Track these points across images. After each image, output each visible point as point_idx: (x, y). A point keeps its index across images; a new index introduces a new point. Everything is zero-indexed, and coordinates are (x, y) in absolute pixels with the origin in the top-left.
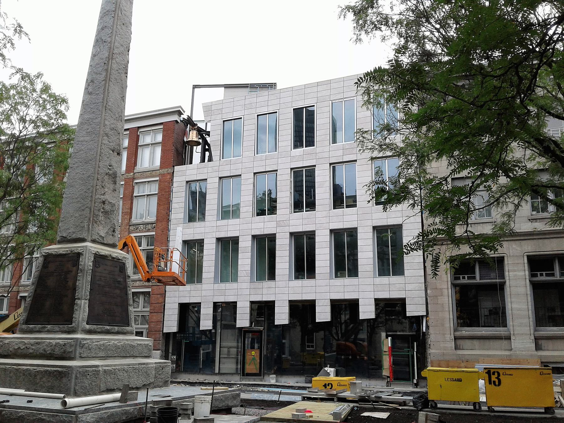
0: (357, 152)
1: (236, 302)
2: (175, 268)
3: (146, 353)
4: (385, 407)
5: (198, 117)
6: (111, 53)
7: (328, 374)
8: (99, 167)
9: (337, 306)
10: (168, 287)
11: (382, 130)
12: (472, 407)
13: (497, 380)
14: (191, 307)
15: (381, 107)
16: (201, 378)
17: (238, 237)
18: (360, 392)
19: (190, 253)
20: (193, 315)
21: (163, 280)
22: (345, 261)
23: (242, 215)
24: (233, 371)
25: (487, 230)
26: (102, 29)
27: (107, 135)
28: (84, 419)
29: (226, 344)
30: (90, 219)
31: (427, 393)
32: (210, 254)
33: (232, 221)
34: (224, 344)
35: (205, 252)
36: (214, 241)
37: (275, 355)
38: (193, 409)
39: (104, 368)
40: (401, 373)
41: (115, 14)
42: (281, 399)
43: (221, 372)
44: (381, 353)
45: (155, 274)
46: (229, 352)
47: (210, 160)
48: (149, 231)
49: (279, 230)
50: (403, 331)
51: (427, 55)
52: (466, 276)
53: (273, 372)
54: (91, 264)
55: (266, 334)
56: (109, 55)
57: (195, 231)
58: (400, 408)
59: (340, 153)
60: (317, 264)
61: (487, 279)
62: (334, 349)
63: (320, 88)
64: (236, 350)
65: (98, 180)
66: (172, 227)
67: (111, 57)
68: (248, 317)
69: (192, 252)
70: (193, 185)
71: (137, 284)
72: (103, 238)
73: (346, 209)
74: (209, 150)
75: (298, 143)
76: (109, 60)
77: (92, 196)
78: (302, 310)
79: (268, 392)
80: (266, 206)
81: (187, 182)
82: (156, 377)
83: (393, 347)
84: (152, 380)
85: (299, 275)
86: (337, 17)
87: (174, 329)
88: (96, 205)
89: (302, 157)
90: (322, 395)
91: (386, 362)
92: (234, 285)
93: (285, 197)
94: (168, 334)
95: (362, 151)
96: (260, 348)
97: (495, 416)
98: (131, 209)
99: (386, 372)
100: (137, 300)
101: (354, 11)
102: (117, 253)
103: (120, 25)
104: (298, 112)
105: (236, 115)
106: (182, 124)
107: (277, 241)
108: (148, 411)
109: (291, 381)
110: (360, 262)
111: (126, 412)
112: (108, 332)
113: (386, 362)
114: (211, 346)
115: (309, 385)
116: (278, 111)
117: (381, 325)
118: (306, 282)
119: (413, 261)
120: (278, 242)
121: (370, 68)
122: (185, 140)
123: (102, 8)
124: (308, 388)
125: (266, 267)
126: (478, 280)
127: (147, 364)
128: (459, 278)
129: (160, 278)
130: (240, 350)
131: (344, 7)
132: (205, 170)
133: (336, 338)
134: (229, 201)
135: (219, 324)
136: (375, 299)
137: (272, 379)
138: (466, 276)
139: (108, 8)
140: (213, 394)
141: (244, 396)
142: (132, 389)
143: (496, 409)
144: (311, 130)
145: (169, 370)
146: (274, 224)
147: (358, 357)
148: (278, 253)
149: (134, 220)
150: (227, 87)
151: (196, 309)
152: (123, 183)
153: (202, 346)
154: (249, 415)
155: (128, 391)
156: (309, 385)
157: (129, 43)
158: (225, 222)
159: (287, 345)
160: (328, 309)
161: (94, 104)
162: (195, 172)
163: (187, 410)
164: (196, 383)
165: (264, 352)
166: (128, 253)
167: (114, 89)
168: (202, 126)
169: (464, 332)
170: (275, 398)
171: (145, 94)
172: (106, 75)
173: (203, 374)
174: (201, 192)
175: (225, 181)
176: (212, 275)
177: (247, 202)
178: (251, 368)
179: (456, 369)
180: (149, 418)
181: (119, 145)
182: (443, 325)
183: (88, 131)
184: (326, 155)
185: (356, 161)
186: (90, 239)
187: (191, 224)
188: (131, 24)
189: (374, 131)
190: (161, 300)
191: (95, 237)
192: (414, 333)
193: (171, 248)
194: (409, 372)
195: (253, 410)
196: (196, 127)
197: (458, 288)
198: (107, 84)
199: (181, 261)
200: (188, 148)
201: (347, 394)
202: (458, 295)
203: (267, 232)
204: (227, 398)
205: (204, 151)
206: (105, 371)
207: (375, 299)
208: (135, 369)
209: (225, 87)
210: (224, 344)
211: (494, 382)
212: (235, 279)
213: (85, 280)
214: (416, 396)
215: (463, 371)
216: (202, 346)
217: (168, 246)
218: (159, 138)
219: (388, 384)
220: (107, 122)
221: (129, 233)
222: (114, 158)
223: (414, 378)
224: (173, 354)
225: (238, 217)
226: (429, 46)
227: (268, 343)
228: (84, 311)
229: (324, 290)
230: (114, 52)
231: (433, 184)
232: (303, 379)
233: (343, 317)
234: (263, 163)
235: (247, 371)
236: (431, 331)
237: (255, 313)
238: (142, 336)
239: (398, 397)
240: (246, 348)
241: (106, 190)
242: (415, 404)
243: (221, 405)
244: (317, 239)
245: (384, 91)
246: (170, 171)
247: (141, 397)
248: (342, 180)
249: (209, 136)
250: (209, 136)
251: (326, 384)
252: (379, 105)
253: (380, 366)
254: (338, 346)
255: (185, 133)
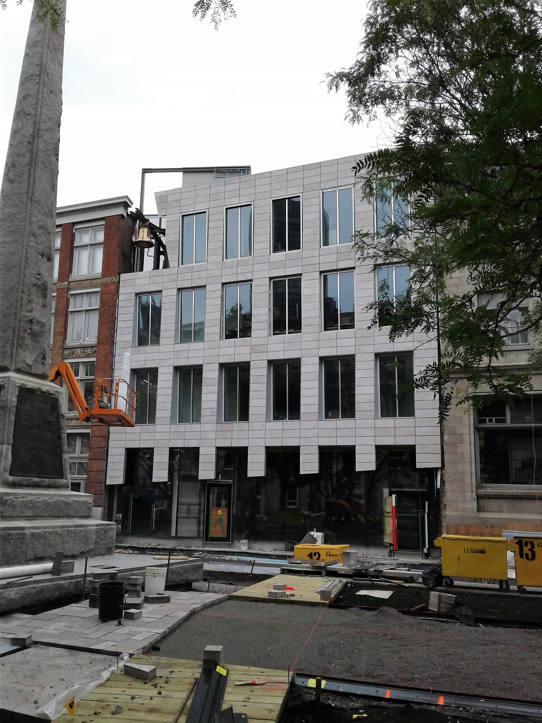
0: (354, 262)
1: (198, 448)
2: (122, 405)
3: (84, 512)
4: (386, 584)
5: (150, 209)
6: (36, 129)
7: (314, 540)
8: (24, 276)
9: (326, 454)
10: (112, 429)
11: (388, 233)
12: (497, 586)
13: (530, 553)
14: (141, 454)
15: (386, 200)
16: (153, 542)
17: (202, 365)
18: (355, 565)
19: (140, 384)
20: (144, 464)
21: (106, 419)
22: (339, 399)
23: (206, 337)
24: (195, 534)
25: (522, 360)
26: (24, 98)
27: (34, 235)
28: (6, 595)
29: (186, 500)
30: (13, 343)
31: (440, 566)
32: (166, 387)
33: (193, 345)
34: (182, 500)
35: (160, 384)
36: (171, 370)
37: (247, 514)
38: (144, 583)
39: (32, 531)
40: (408, 541)
41: (40, 79)
42: (254, 572)
43: (178, 535)
44: (383, 514)
45: (96, 411)
46: (188, 509)
47: (166, 265)
48: (88, 356)
49: (254, 357)
50: (411, 486)
51: (446, 134)
52: (494, 419)
53: (244, 535)
54: (15, 399)
55: (235, 488)
56: (34, 132)
57: (146, 357)
58: (406, 585)
59: (334, 258)
60: (303, 401)
61: (521, 423)
62: (323, 507)
63: (307, 174)
64: (197, 507)
65: (23, 292)
66: (117, 351)
67: (36, 134)
68: (213, 466)
69: (142, 383)
70: (144, 299)
71: (74, 423)
72: (30, 366)
73: (340, 331)
74: (165, 253)
75: (279, 245)
76: (34, 137)
77: (16, 314)
78: (282, 459)
79: (239, 562)
80: (238, 325)
81: (137, 294)
82: (96, 543)
83: (399, 507)
84: (92, 547)
85: (279, 414)
86: (327, 89)
87: (120, 481)
88: (21, 325)
89: (285, 263)
90: (306, 567)
91: (389, 525)
92: (196, 427)
93: (262, 314)
94: (112, 487)
95: (362, 260)
96: (228, 506)
97: (526, 598)
98: (66, 328)
99: (388, 539)
100: (73, 443)
101: (349, 80)
102: (48, 386)
103: (47, 93)
104: (278, 205)
105: (199, 208)
106: (130, 221)
107: (251, 370)
108: (86, 585)
109: (267, 548)
110: (358, 399)
111: (60, 587)
112: (36, 486)
113: (389, 525)
114: (166, 501)
115: (291, 554)
116: (252, 203)
117: (383, 478)
118: (288, 424)
119: (425, 400)
120: (253, 372)
121: (374, 149)
122: (134, 240)
123: (23, 72)
124: (290, 557)
125: (237, 404)
126: (509, 424)
127: (86, 526)
128: (485, 421)
129: (103, 417)
130: (203, 507)
131: (334, 75)
132: (160, 279)
133: (325, 493)
134: (190, 319)
135: (176, 475)
136: (376, 446)
137: (243, 546)
138: (494, 419)
139: (30, 72)
140: (168, 565)
141: (208, 567)
142: (67, 557)
143: (528, 589)
144: (295, 228)
145: (113, 534)
146: (247, 350)
147: (353, 519)
148: (252, 387)
149: (69, 342)
150: (187, 171)
151: (148, 456)
152: (54, 294)
153: (155, 502)
154: (215, 592)
155: (62, 561)
156: (291, 554)
157: (60, 117)
158: (184, 346)
159: (262, 502)
160: (316, 458)
161: (17, 194)
162: (146, 281)
163: (135, 585)
164: (147, 548)
165: (234, 511)
166: (61, 385)
167: (41, 174)
168: (155, 222)
169: (489, 490)
170: (247, 569)
171: (88, 174)
172: (31, 158)
173: (155, 538)
174: (154, 307)
175: (185, 293)
176: (168, 413)
177: (213, 320)
178: (216, 531)
179: (478, 538)
180: (88, 595)
181: (50, 248)
182: (462, 480)
183: (9, 229)
184: (315, 260)
185: (354, 268)
186: (13, 367)
187: (142, 348)
188: (61, 91)
189: (378, 233)
190: (103, 444)
191: (20, 365)
192: (426, 490)
193: (116, 378)
194: (419, 537)
195: (218, 585)
196: (148, 224)
197: (482, 433)
198: (33, 169)
199: (129, 395)
200: (138, 250)
201: (339, 566)
202: (483, 442)
203: (238, 359)
204: (186, 570)
205: (158, 254)
206: (33, 535)
207: (376, 446)
208: (71, 532)
209: (184, 172)
210: (182, 500)
211: (527, 555)
212: (197, 418)
213: (7, 421)
214: (427, 570)
215: (487, 541)
216: (155, 502)
217: (112, 376)
218: (101, 237)
219: (391, 554)
220: (33, 219)
221: (63, 358)
222: (44, 265)
223: (424, 546)
224: (118, 512)
225: (202, 339)
226: (448, 122)
227: (239, 499)
228: (6, 459)
229: (311, 434)
230: (41, 128)
231: (454, 305)
232: (282, 545)
233: (334, 468)
234: (234, 271)
235: (212, 534)
236: (447, 487)
237: (222, 462)
238: (79, 491)
239: (403, 571)
240: (211, 506)
241: (34, 305)
242: (425, 581)
243: (179, 579)
244: (303, 369)
245: (390, 179)
246: (115, 279)
247: (79, 568)
248: (336, 290)
249: (164, 235)
250: (164, 235)
251: (311, 554)
252: (384, 198)
253: (381, 531)
254: (328, 504)
255: (133, 231)
